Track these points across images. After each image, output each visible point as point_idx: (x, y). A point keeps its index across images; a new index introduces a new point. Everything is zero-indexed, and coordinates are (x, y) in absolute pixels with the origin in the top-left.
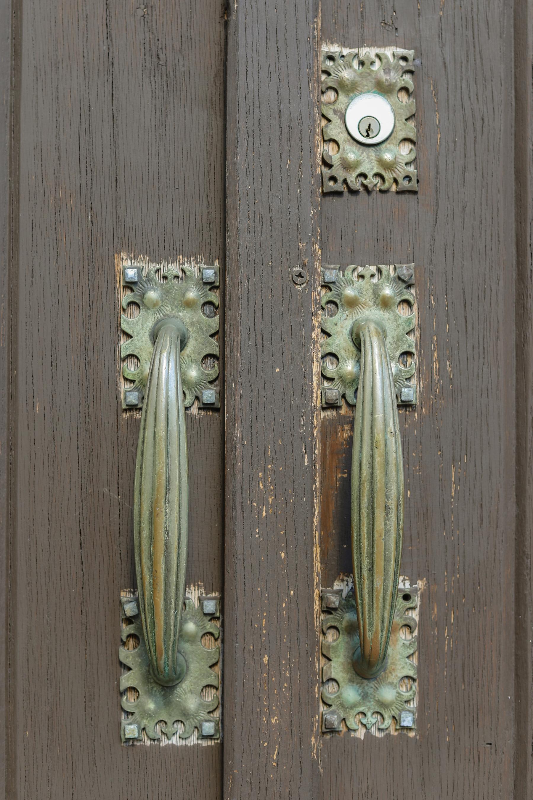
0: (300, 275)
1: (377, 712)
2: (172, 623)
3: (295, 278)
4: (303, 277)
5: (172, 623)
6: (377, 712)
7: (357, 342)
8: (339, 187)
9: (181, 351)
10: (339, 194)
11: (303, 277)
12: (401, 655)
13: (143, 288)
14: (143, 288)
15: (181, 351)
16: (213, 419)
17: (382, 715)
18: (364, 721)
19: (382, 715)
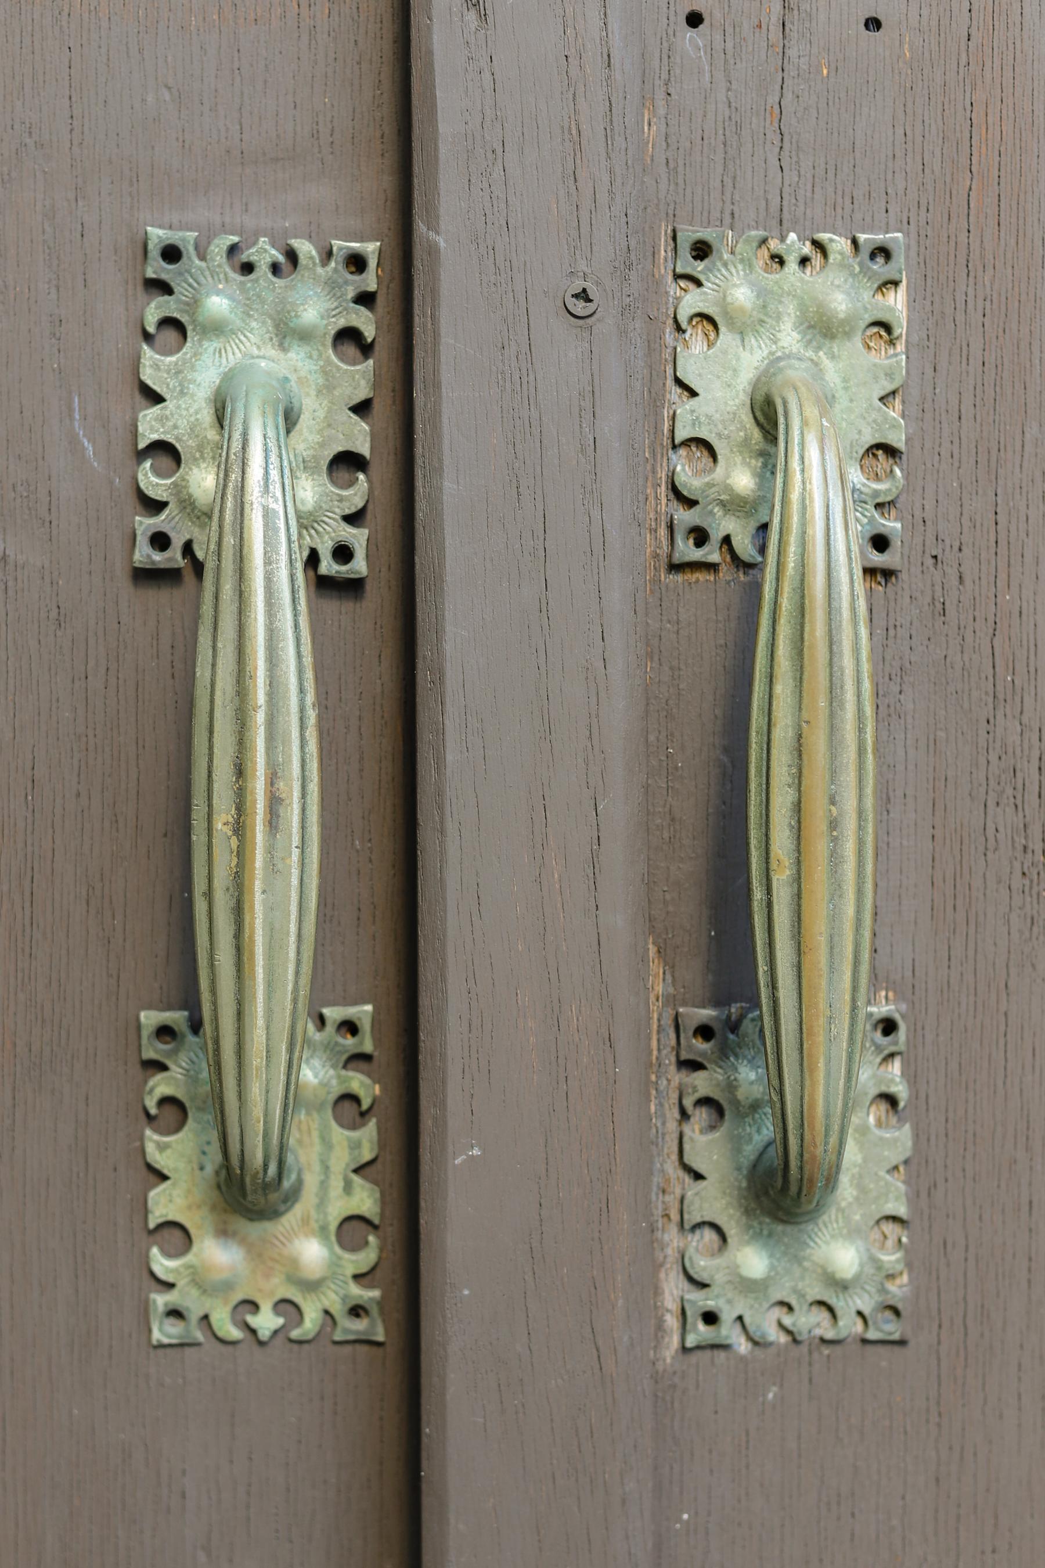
0: (669, 622)
1: (821, 1303)
2: (870, 757)
3: (571, 302)
4: (591, 301)
5: (870, 757)
6: (821, 1303)
7: (767, 416)
8: (712, 553)
9: (288, 432)
10: (711, 567)
11: (591, 301)
12: (868, 1163)
13: (195, 285)
14: (195, 285)
15: (288, 432)
16: (382, 592)
17: (831, 1309)
18: (787, 1321)
19: (831, 1309)
